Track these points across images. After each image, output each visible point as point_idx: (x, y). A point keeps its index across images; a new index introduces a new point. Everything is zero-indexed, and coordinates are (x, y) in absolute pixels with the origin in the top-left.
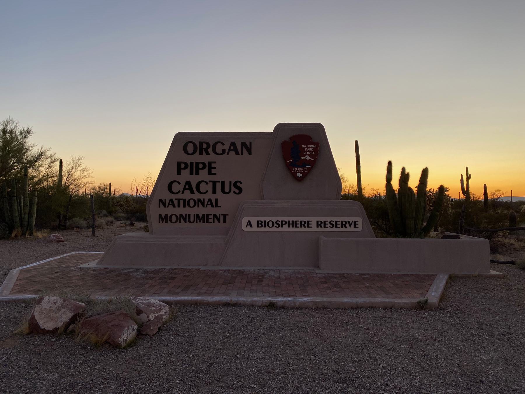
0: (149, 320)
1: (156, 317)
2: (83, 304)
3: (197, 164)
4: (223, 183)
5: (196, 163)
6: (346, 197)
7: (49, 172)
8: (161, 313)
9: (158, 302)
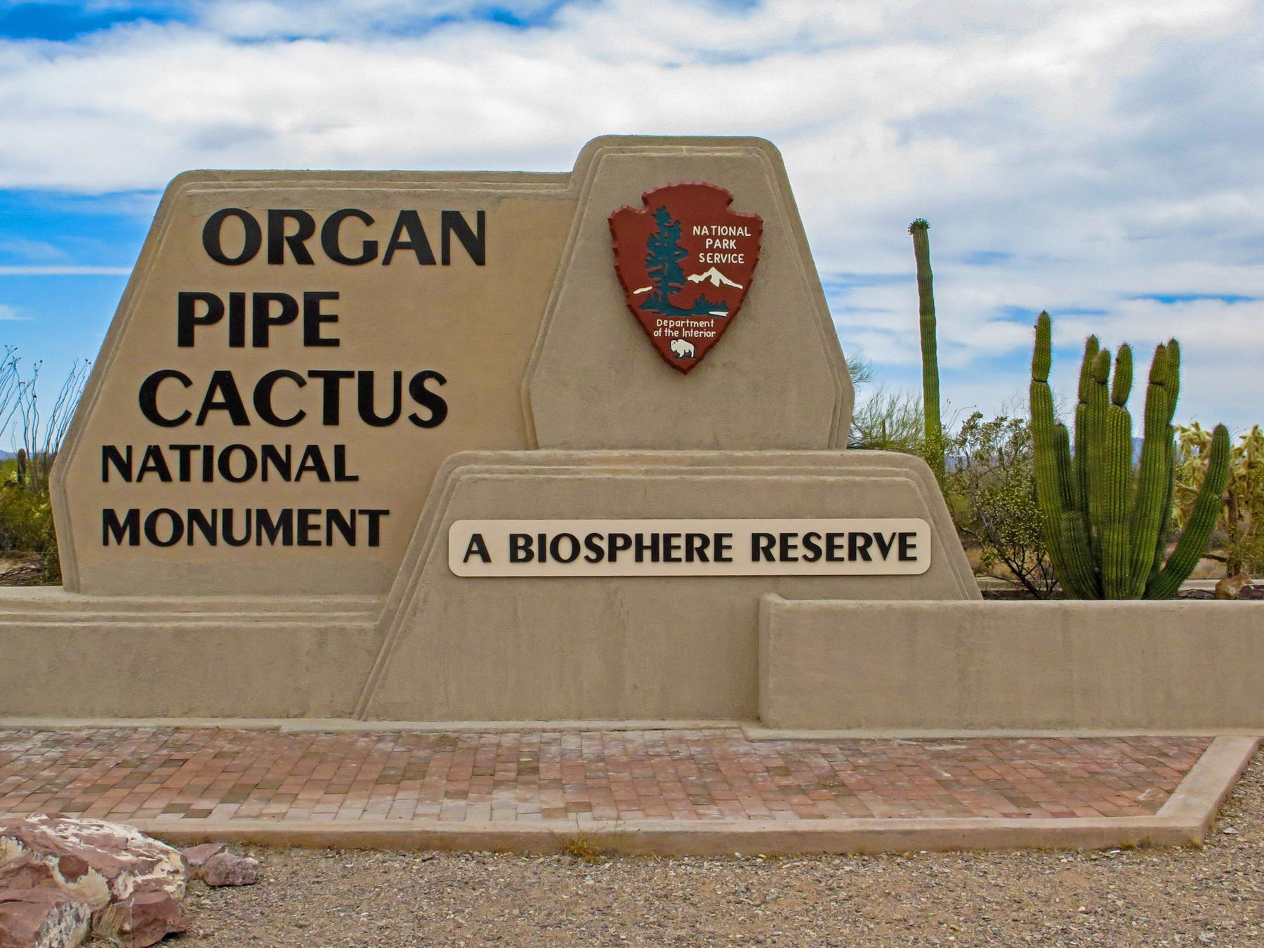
3: (261, 301)
4: (366, 381)
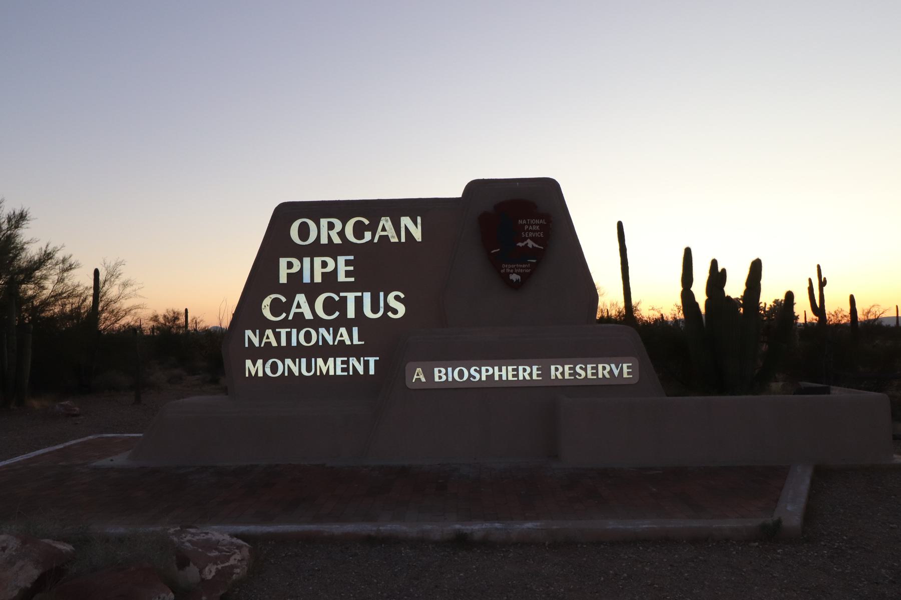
0: (203, 580)
1: (218, 571)
2: (67, 548)
6: (607, 320)
7: (60, 288)
8: (232, 562)
9: (227, 538)
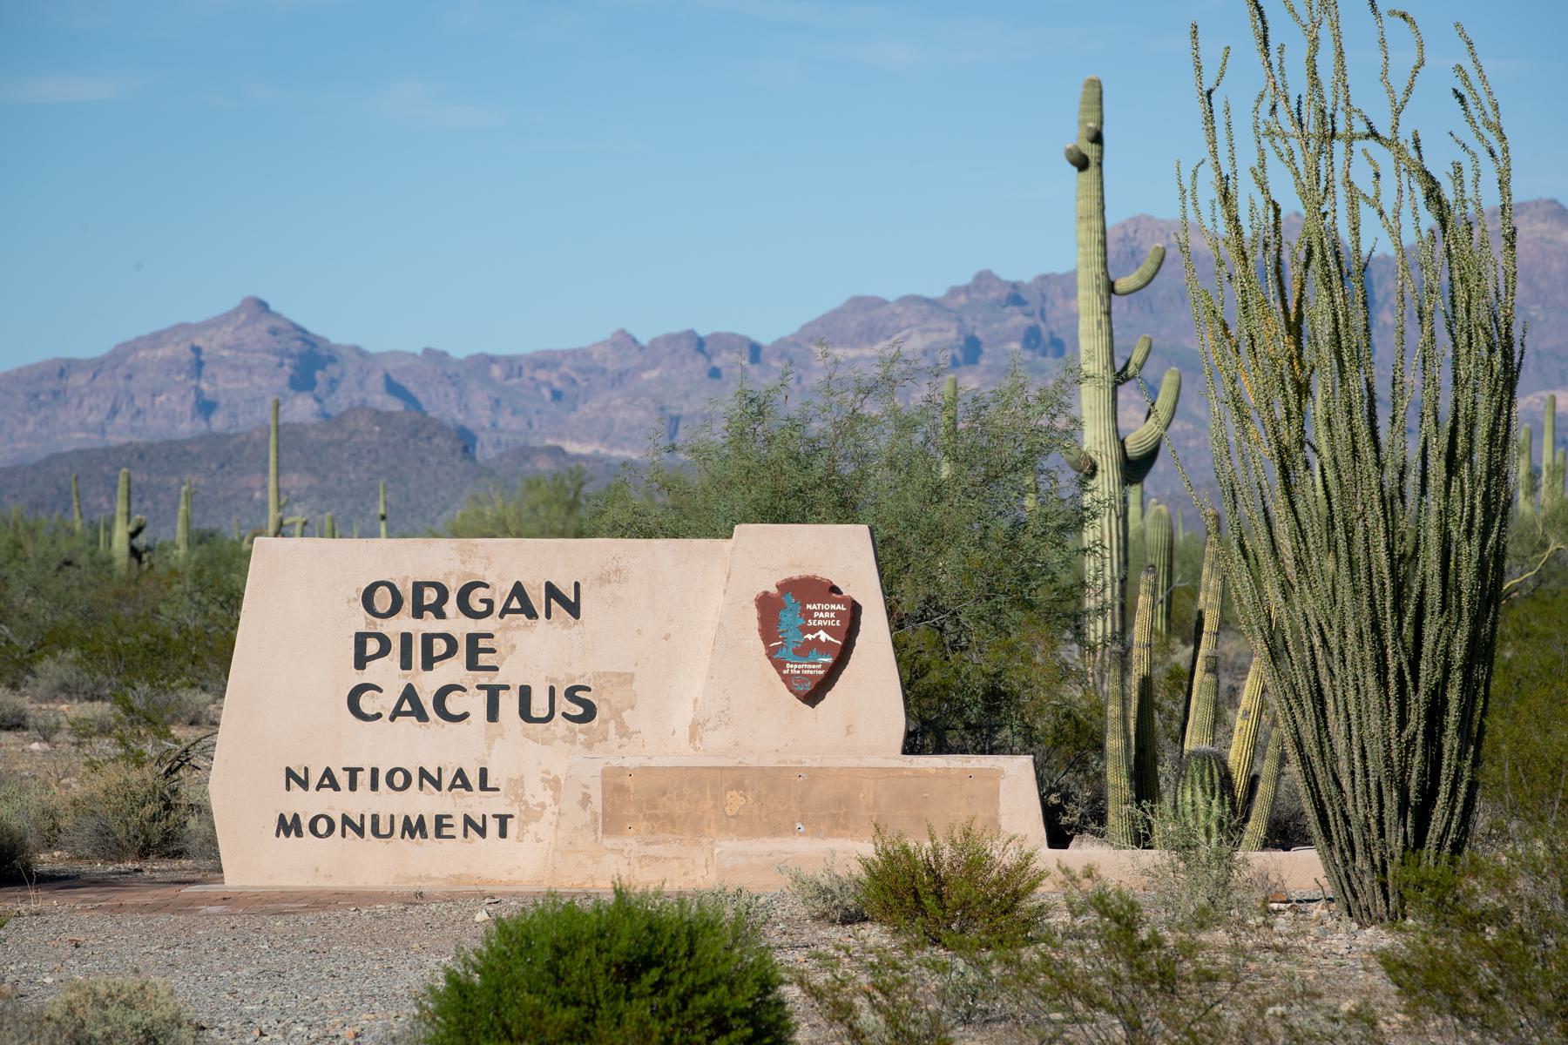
3: (428, 639)
4: (525, 693)
5: (424, 636)
